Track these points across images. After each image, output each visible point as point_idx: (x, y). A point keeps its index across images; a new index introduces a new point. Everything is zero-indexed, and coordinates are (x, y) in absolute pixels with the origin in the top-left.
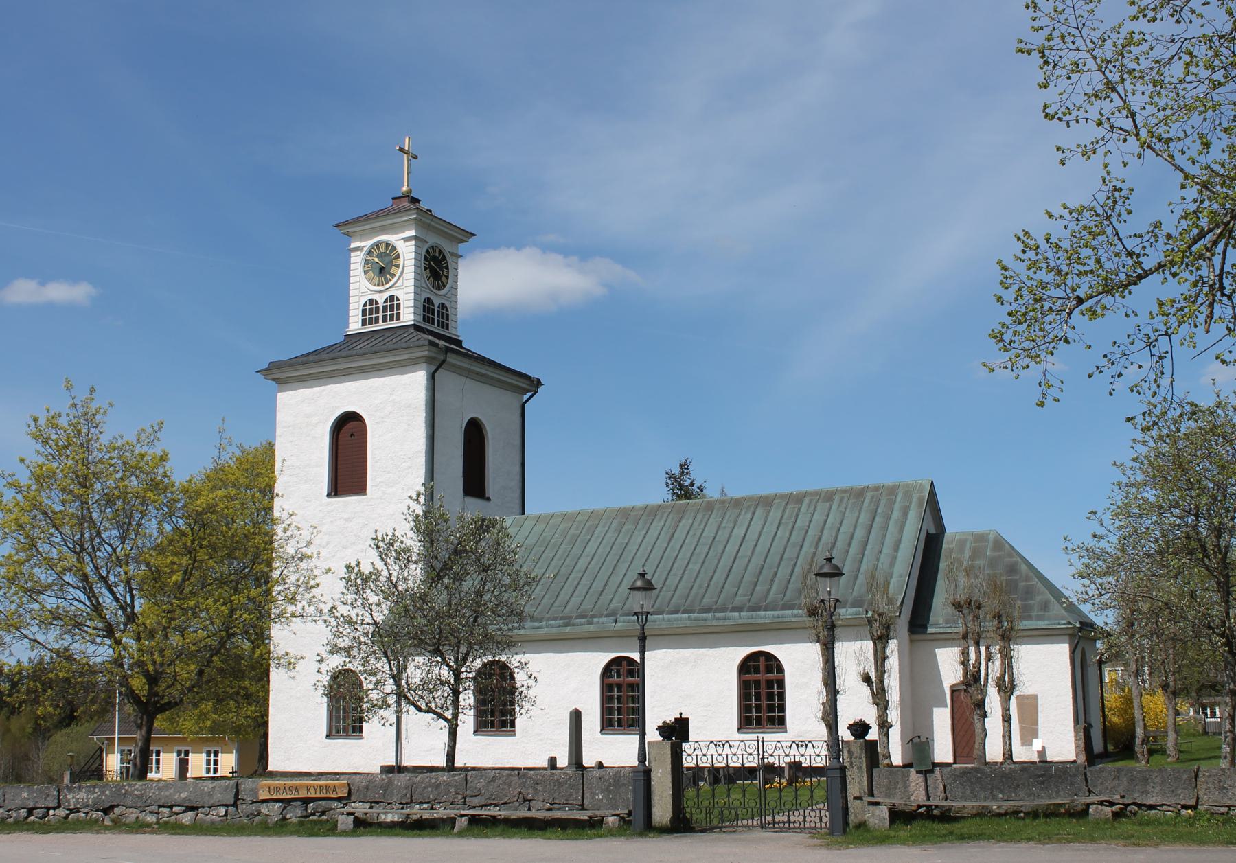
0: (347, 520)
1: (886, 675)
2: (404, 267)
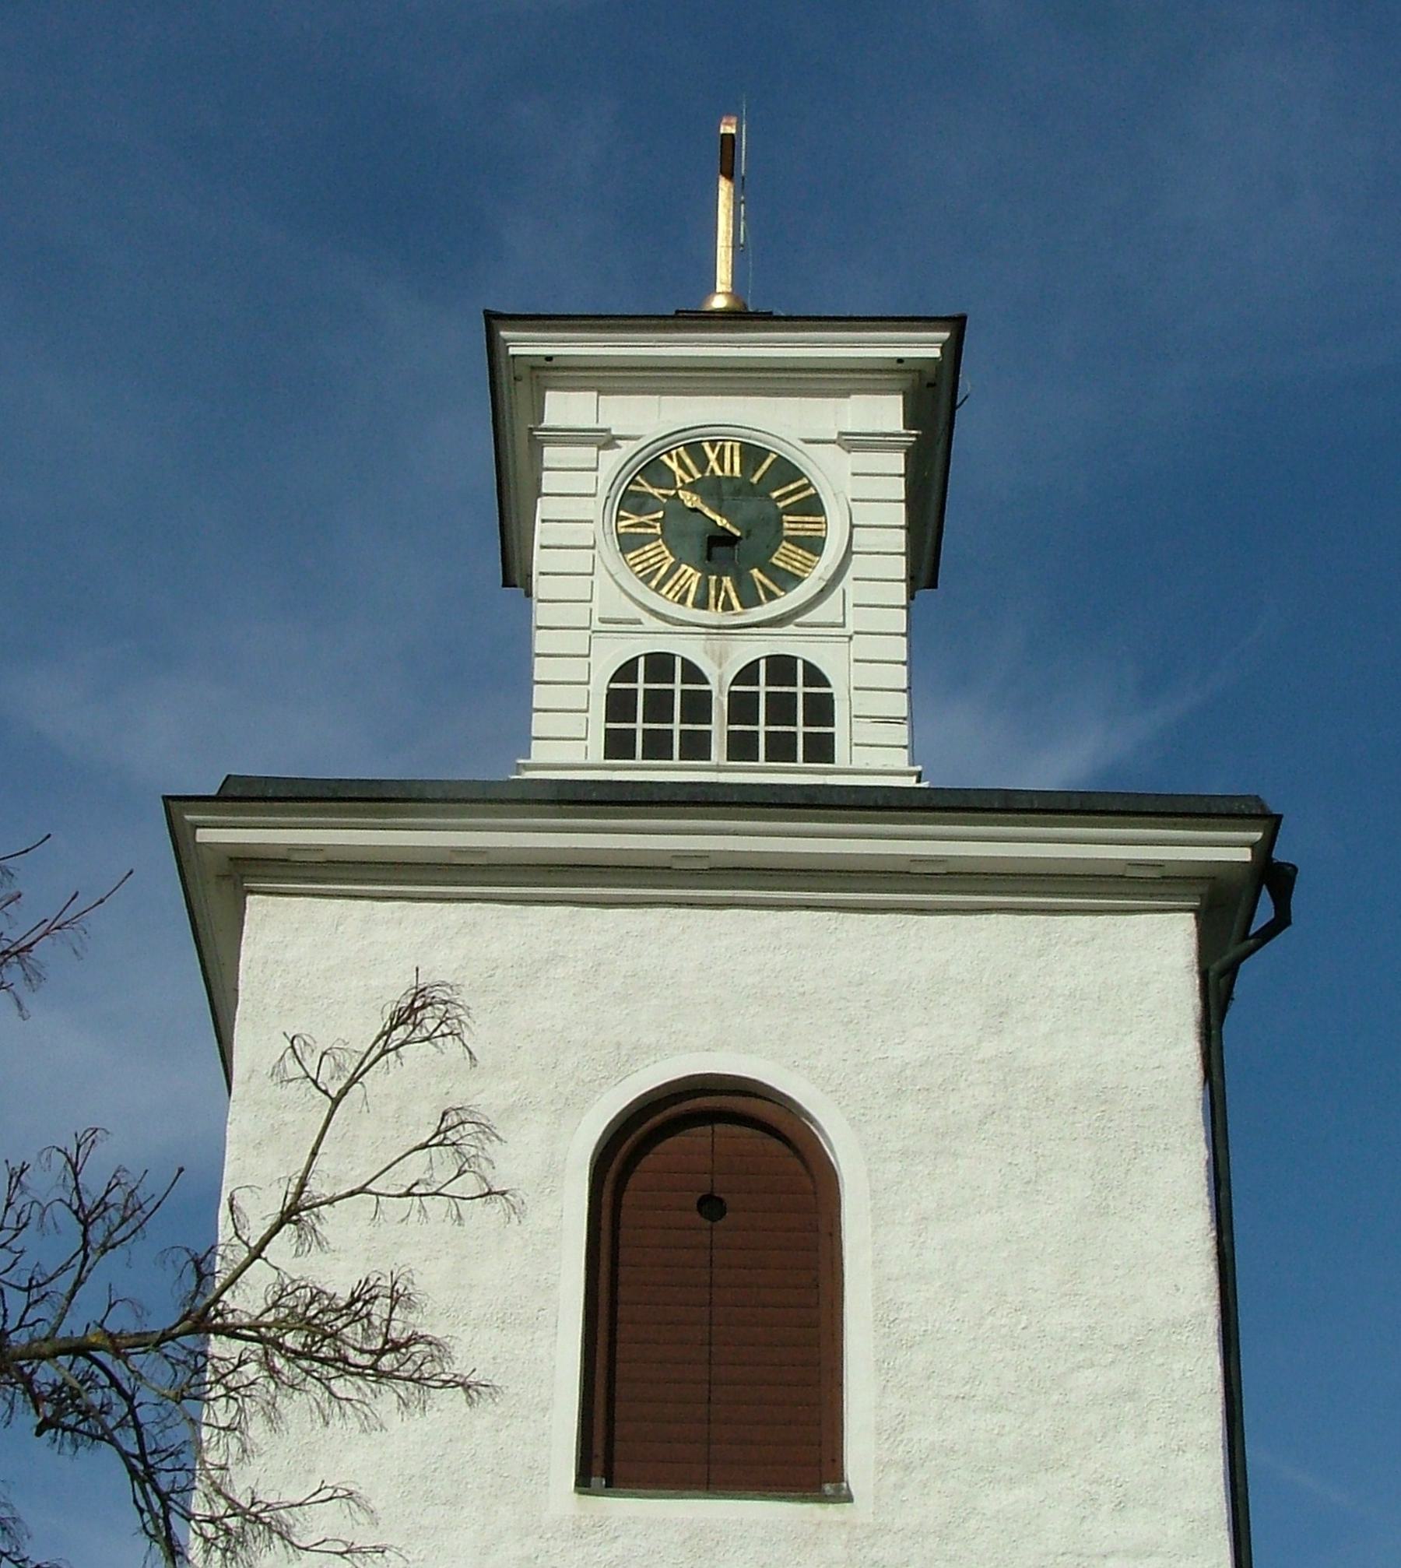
1: (618, 548)
2: (849, 552)
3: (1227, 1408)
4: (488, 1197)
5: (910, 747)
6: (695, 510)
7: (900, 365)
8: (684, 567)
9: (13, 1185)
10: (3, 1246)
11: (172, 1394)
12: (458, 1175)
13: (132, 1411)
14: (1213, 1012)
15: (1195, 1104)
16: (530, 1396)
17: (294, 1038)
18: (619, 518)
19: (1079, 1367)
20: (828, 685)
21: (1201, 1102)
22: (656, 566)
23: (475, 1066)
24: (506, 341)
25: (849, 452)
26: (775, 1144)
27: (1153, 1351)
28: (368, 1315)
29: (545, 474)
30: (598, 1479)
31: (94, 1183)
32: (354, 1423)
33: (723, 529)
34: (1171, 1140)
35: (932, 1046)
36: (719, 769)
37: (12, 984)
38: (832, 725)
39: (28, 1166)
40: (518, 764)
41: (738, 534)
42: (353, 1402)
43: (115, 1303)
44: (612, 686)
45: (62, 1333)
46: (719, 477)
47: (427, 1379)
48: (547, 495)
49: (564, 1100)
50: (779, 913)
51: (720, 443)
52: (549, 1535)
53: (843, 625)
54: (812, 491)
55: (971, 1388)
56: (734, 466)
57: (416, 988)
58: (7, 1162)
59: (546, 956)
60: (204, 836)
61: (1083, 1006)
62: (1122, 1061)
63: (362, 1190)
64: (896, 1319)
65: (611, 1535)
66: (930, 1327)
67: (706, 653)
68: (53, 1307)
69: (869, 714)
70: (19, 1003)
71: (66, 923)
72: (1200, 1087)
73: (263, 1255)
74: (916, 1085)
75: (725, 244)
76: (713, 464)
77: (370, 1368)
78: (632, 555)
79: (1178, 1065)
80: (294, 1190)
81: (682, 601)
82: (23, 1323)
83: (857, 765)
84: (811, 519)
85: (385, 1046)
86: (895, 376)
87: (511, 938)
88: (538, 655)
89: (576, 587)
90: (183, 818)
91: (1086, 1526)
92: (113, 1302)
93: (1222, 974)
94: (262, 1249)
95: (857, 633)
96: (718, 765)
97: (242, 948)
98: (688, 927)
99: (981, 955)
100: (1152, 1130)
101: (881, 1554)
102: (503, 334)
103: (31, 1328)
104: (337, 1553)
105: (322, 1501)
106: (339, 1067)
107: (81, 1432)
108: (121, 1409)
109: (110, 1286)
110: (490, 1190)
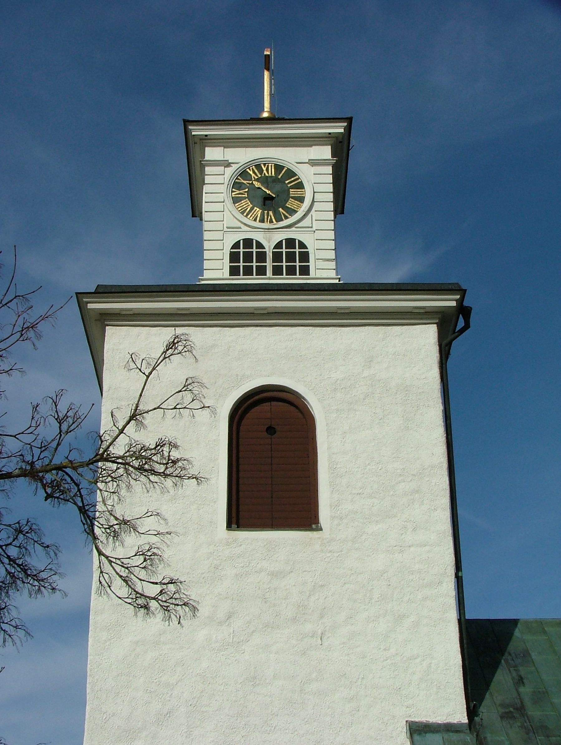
0: (275, 575)
1: (232, 202)
2: (313, 202)
3: (451, 494)
4: (203, 409)
5: (337, 269)
6: (259, 188)
7: (330, 135)
8: (255, 208)
9: (34, 411)
10: (1, 540)
11: (93, 481)
12: (193, 401)
13: (79, 490)
14: (444, 356)
15: (438, 390)
16: (210, 497)
17: (132, 354)
18: (232, 192)
19: (400, 482)
20: (307, 248)
21: (440, 390)
22: (246, 208)
23: (197, 362)
24: (191, 130)
25: (312, 166)
26: (292, 408)
27: (425, 476)
28: (162, 451)
29: (206, 177)
30: (234, 525)
31: (63, 408)
32: (158, 491)
33: (269, 194)
34: (430, 403)
35: (347, 373)
36: (269, 279)
37: (31, 338)
38: (309, 262)
39: (39, 404)
40: (199, 279)
41: (274, 196)
42: (158, 483)
43: (72, 450)
44: (232, 250)
45: (54, 462)
46: (267, 176)
47: (183, 476)
48: (207, 184)
49: (219, 395)
50: (292, 328)
51: (267, 164)
52: (218, 545)
53: (312, 227)
54: (300, 180)
55: (362, 491)
56: (272, 172)
57: (175, 335)
58: (31, 403)
59: (211, 345)
60: (90, 306)
61: (398, 358)
62: (413, 376)
63: (158, 408)
64: (336, 467)
65: (239, 544)
66: (348, 470)
67: (264, 238)
68: (50, 452)
69: (321, 258)
70: (34, 345)
71: (49, 315)
72: (440, 385)
73: (124, 432)
74: (341, 387)
75: (267, 94)
76: (265, 172)
77: (162, 473)
78: (237, 204)
79: (432, 377)
80: (134, 408)
81: (255, 220)
82: (40, 458)
83: (318, 276)
84: (300, 190)
85: (165, 356)
86: (326, 139)
87: (199, 339)
88: (205, 240)
89: (218, 216)
90: (83, 300)
91: (403, 536)
92: (71, 449)
93: (446, 345)
94: (123, 430)
95: (316, 230)
96: (269, 277)
97: (105, 345)
98: (261, 334)
99: (363, 341)
100: (423, 400)
101: (333, 548)
102: (190, 127)
103: (42, 460)
104: (154, 535)
105: (148, 517)
106: (148, 364)
107: (61, 499)
108: (75, 490)
109: (70, 444)
110: (204, 406)
